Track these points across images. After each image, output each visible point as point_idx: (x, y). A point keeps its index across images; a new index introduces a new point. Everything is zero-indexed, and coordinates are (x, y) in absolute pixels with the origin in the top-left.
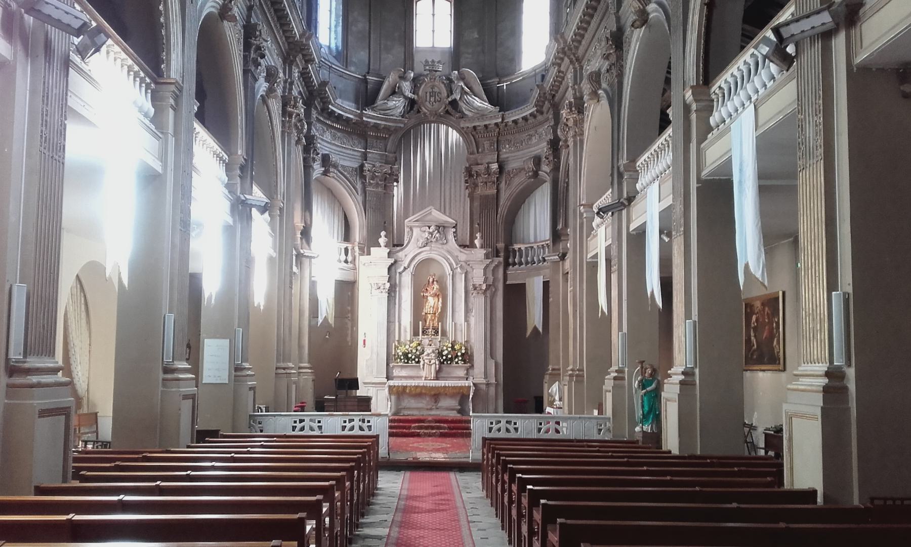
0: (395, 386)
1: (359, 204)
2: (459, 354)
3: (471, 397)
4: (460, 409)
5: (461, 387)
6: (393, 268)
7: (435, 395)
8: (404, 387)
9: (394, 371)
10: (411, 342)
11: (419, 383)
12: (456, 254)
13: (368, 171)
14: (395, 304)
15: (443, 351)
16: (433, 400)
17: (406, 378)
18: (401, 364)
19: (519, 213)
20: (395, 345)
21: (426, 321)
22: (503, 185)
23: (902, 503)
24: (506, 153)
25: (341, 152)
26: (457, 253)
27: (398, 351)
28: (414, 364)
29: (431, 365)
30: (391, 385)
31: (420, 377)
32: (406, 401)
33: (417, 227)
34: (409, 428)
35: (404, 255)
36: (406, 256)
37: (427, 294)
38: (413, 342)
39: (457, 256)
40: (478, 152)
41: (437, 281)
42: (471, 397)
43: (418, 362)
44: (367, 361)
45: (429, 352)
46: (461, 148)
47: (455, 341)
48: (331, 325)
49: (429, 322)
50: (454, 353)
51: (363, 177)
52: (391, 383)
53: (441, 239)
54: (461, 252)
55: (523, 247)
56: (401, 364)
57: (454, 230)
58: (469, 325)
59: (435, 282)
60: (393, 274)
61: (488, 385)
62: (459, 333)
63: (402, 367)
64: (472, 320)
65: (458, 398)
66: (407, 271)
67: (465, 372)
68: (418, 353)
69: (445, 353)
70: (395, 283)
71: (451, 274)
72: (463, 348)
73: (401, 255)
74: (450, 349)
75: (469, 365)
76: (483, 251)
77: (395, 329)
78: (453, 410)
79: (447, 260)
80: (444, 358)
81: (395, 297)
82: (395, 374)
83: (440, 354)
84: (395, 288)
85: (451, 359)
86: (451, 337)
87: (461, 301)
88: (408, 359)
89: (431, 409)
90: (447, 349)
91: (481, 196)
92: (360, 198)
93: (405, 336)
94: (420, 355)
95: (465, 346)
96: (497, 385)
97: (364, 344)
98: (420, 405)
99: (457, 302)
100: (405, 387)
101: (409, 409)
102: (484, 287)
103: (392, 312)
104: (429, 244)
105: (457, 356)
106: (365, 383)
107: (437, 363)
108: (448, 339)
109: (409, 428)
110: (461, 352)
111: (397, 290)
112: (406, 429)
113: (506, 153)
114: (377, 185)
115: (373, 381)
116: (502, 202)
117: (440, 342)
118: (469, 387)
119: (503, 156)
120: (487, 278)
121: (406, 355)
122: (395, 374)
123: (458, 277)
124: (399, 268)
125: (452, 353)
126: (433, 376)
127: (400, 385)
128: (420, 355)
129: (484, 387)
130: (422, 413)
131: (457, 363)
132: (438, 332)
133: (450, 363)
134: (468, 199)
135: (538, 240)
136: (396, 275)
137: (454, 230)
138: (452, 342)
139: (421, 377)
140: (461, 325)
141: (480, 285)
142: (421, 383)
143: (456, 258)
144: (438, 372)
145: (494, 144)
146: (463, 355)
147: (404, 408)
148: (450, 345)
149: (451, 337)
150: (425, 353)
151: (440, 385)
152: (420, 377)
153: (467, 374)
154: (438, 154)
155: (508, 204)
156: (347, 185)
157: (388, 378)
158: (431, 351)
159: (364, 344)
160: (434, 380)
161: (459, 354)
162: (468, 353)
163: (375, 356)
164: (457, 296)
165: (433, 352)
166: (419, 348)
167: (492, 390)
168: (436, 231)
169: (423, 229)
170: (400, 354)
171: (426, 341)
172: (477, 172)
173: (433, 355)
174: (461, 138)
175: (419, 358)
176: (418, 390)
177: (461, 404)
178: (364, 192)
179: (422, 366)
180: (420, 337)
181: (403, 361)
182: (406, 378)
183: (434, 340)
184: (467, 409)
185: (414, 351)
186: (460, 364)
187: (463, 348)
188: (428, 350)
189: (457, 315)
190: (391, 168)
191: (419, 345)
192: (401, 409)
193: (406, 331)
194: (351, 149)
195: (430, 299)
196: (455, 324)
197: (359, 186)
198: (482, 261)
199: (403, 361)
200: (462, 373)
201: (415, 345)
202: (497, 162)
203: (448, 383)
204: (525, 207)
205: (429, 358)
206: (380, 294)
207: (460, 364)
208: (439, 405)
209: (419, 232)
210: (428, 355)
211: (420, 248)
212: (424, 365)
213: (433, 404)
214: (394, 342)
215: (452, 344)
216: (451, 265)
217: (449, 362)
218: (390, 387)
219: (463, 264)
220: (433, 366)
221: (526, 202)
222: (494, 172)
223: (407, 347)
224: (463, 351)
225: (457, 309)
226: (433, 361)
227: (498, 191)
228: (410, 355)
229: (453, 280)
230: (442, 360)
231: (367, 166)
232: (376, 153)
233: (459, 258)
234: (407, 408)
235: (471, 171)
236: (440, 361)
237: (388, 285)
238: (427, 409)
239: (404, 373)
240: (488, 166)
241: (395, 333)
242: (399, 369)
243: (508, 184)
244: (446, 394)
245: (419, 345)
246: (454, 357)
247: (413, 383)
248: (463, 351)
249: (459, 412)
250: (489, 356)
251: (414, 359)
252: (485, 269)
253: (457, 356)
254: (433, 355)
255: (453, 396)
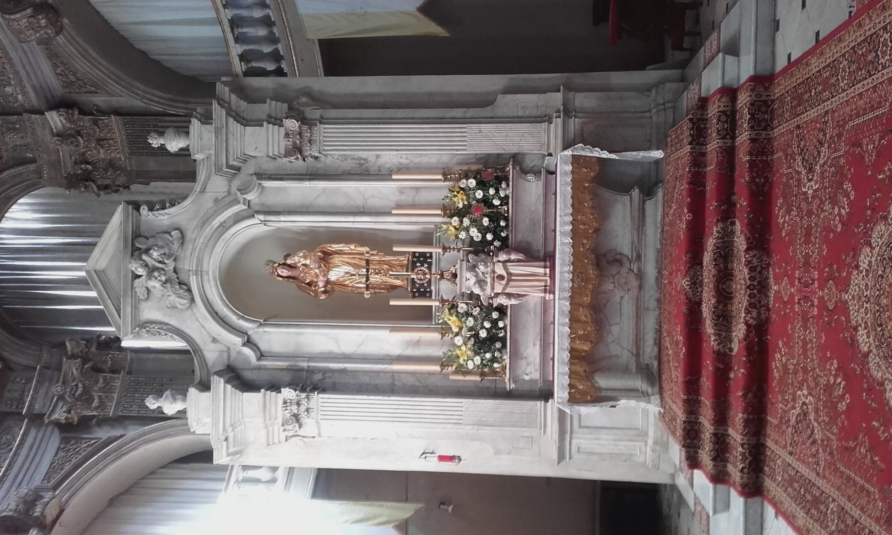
0: (570, 385)
1: (144, 434)
2: (479, 194)
3: (605, 155)
4: (641, 191)
5: (576, 185)
6: (248, 375)
7: (598, 265)
8: (572, 357)
9: (527, 378)
10: (445, 329)
11: (562, 312)
12: (210, 204)
13: (69, 412)
14: (344, 371)
15: (472, 242)
16: (614, 270)
17: (546, 344)
18: (506, 358)
19: (169, 65)
20: (456, 372)
21: (394, 287)
22: (100, 100)
23: (501, 329)
24: (24, 93)
25: (17, 476)
26: (208, 201)
27: (470, 365)
28: (508, 322)
29: (510, 274)
30: (566, 395)
31: (545, 307)
32: (614, 349)
33: (135, 308)
34: (723, 359)
35: (213, 346)
36: (214, 340)
37: (321, 284)
38: (445, 323)
39: (216, 201)
40: (32, 161)
41: (287, 256)
42: (605, 155)
43: (501, 310)
44: (498, 452)
45: (473, 280)
46: (53, 201)
47: (444, 208)
48: (417, 512)
49: (397, 277)
50: (477, 209)
51: (85, 424)
52: (561, 393)
53: (168, 244)
54: (203, 191)
55: (236, 50)
56: (506, 358)
57: (144, 210)
58: (402, 169)
59: (289, 262)
60: (263, 376)
61: (567, 111)
62: (425, 197)
63: (515, 355)
64: (389, 158)
65: (607, 194)
66: (255, 338)
67: (530, 177)
68: (476, 311)
69: (475, 233)
70: (288, 369)
71: (262, 217)
72: (463, 183)
73: (212, 354)
74: (466, 222)
75: (510, 168)
76: (195, 125)
77: (413, 373)
78: (642, 211)
79: (224, 227)
80: (489, 237)
81: (325, 371)
82: (536, 375)
83: (479, 249)
84: (301, 370)
85: (495, 218)
86: (434, 218)
87: (338, 189)
88: (492, 338)
89: (640, 276)
90: (467, 230)
91: (132, 154)
92: (133, 431)
93: (431, 343)
94: (481, 306)
95: (460, 179)
96: (569, 88)
97: (451, 458)
98: (628, 308)
99: (341, 201)
100: (575, 356)
101: (638, 341)
102: (292, 124)
103: (365, 379)
104: (183, 277)
105: (486, 201)
106: (561, 457)
107: (503, 257)
108: (438, 226)
109: (723, 359)
110: (475, 190)
111: (304, 365)
112: (728, 368)
113: (24, 93)
114: (107, 389)
115: (556, 436)
116: (137, 103)
117: (445, 249)
118: (576, 159)
119: (34, 100)
120: (269, 116)
121: (481, 345)
122: (536, 375)
123: (272, 200)
124: (246, 360)
125: (477, 215)
126: (542, 270)
127: (567, 369)
128: (481, 306)
129: (574, 124)
130: (653, 304)
131: (505, 201)
132: (423, 255)
133: (506, 219)
134: (153, 184)
135: (213, 15)
136: (265, 369)
137: (144, 210)
138: (445, 215)
139: (545, 303)
140: (401, 191)
141: (287, 135)
142: (561, 305)
143: (220, 204)
144: (530, 255)
145: (9, 123)
146: (482, 184)
147: (638, 355)
148: (455, 221)
149: (434, 218)
150: (477, 291)
151: (569, 250)
152: (545, 307)
153: (537, 173)
154: (64, 251)
155: (142, 87)
156: (96, 463)
157: (546, 395)
158: (469, 275)
159: (451, 458)
160: (553, 268)
161: (479, 194)
162: (478, 172)
163: (487, 431)
164: (322, 201)
165: (473, 268)
166: (462, 307)
167: (584, 100)
168: (144, 257)
169: (141, 292)
170: (477, 360)
171: (445, 288)
172: (75, 163)
173: (482, 268)
174: (21, 201)
175: (490, 308)
176: (583, 314)
177: (624, 189)
178: (119, 420)
179: (513, 302)
180: (435, 304)
181: (497, 354)
182: (546, 344)
183: (443, 265)
184: (637, 172)
185: (470, 322)
186: (509, 192)
187: (463, 183)
188: (469, 282)
189: (375, 202)
190: (69, 358)
191: (453, 307)
192: (638, 362)
193: (418, 343)
194: (15, 454)
195: (333, 275)
196: (399, 206)
197: (103, 433)
198: (217, 131)
199: (497, 354)
200: (533, 188)
201: (454, 318)
202: (41, 113)
203: (565, 224)
204: (154, 50)
205: (489, 280)
206: (313, 414)
207: (509, 192)
208: (626, 250)
209: (149, 303)
210: (481, 283)
211: (193, 300)
212: (509, 296)
213: (624, 270)
214: (448, 375)
215: (451, 216)
216: (238, 218)
217: (502, 224)
218: (575, 398)
219: (236, 183)
220: (515, 269)
221: (132, 42)
222: (70, 121)
223: (459, 341)
224: (472, 183)
225: (359, 202)
226: (500, 270)
227: (118, 112)
228: (483, 334)
229: (278, 213)
230: (497, 243)
231: (60, 415)
232: (36, 391)
233: (220, 196)
234: (638, 347)
235: (76, 175)
236: (500, 249)
237: (288, 393)
238: (641, 287)
239: (532, 351)
240: (58, 135)
241: (422, 373)
242: (523, 363)
243: (97, 88)
244: (597, 231)
245: (453, 307)
246: (487, 211)
247: (561, 330)
248: (472, 183)
249: (648, 192)
250: (487, 112)
251: (494, 323)
252: (245, 122)
253: (486, 201)
254: (482, 268)
255: (602, 212)
